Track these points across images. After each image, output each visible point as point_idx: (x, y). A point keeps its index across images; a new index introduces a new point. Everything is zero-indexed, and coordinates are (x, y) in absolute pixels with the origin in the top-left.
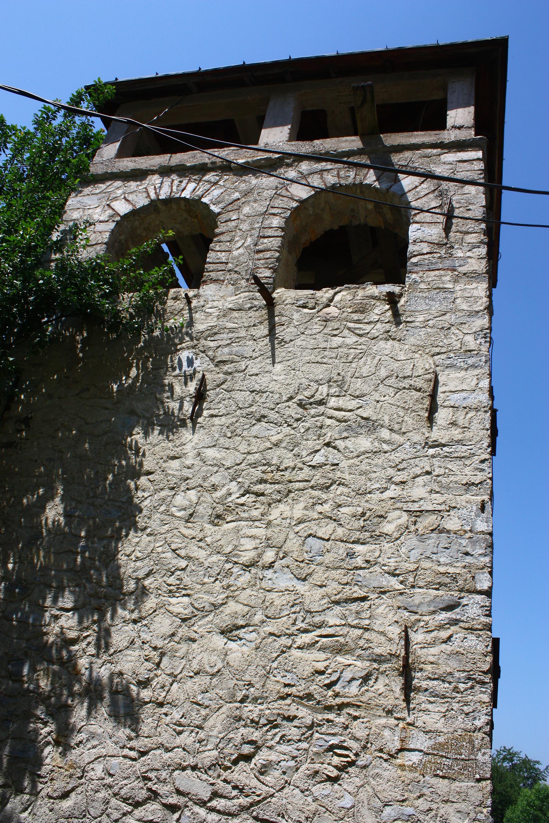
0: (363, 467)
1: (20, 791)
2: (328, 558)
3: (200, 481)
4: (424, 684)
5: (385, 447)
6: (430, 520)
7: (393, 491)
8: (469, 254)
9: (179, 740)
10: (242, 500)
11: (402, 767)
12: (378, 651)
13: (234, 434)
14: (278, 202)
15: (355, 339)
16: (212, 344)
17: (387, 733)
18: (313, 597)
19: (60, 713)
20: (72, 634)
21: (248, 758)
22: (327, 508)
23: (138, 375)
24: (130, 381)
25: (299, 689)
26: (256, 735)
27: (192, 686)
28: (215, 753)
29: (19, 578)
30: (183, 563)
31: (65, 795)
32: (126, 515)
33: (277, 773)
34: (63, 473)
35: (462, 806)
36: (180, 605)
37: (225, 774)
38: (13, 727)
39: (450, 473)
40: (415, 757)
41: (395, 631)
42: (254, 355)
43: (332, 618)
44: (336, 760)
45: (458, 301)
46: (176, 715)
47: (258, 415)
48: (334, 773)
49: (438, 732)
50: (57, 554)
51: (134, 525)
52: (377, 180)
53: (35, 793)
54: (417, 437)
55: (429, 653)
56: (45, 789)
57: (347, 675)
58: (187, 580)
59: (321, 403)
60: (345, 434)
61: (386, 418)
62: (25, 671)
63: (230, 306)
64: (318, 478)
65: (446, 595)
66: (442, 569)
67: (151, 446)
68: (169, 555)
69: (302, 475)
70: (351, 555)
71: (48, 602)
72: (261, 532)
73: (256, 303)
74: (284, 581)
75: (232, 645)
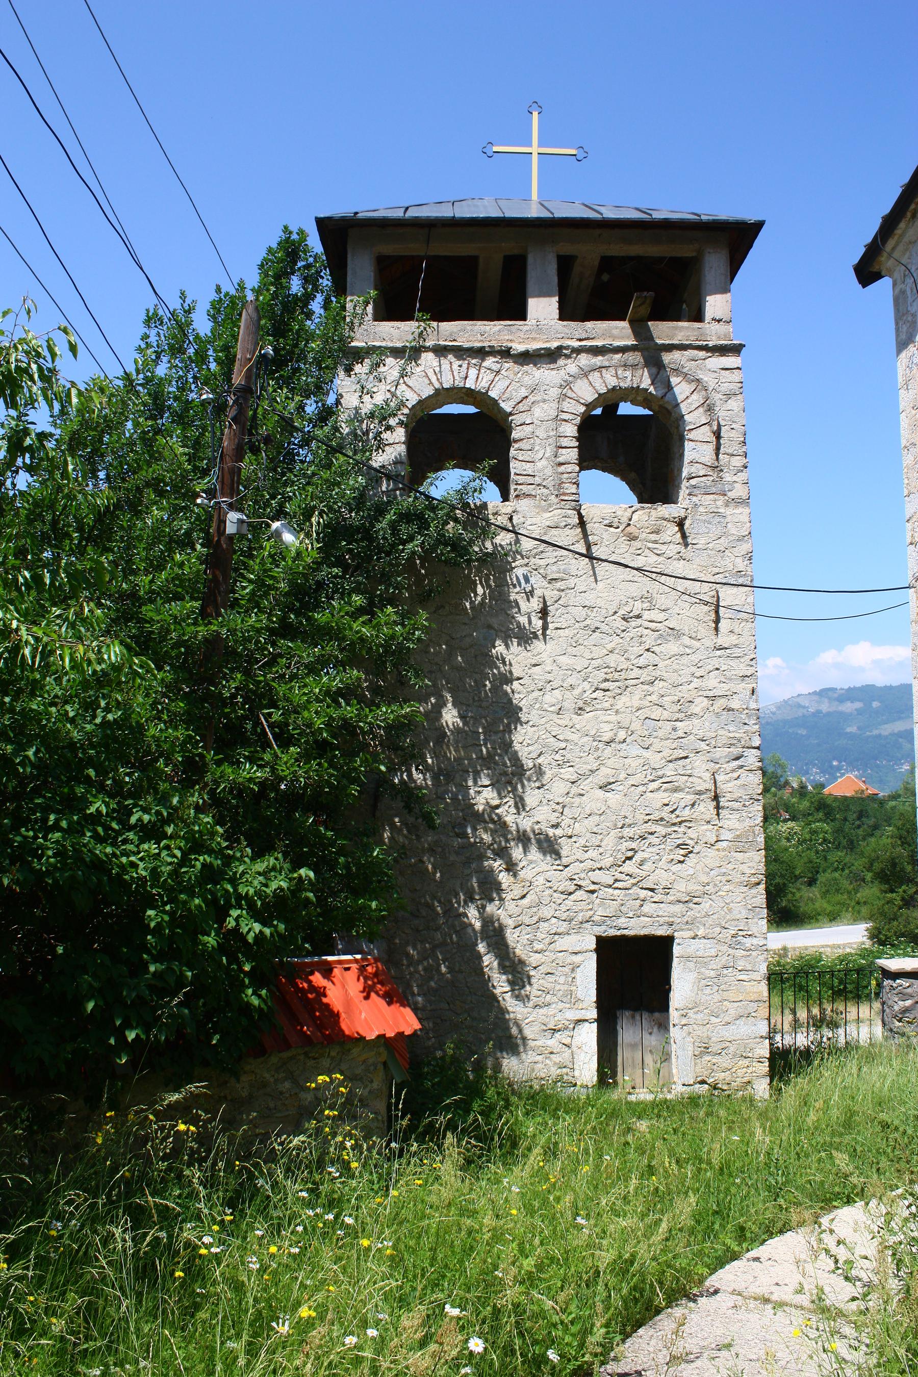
0: (675, 667)
1: (491, 900)
2: (660, 733)
3: (560, 683)
4: (726, 804)
5: (688, 651)
6: (721, 702)
7: (696, 683)
8: (735, 478)
9: (587, 855)
10: (594, 695)
11: (718, 850)
12: (698, 788)
13: (578, 644)
14: (567, 405)
15: (656, 558)
16: (542, 562)
17: (708, 833)
18: (656, 760)
19: (502, 853)
20: (496, 802)
21: (630, 858)
22: (654, 698)
23: (484, 593)
24: (479, 599)
25: (656, 815)
26: (634, 845)
27: (591, 822)
28: (611, 859)
29: (440, 768)
30: (563, 745)
31: (523, 897)
32: (510, 714)
33: (650, 864)
34: (447, 683)
35: (751, 864)
36: (568, 773)
37: (620, 869)
38: (474, 866)
39: (732, 668)
40: (725, 844)
41: (707, 776)
42: (580, 573)
43: (669, 770)
44: (682, 852)
45: (729, 525)
46: (582, 841)
47: (593, 628)
48: (682, 859)
49: (737, 830)
50: (464, 747)
51: (518, 720)
52: (653, 384)
53: (501, 900)
54: (709, 643)
55: (728, 787)
56: (508, 896)
57: (682, 804)
58: (569, 756)
59: (638, 617)
60: (659, 642)
61: (686, 628)
62: (469, 831)
63: (548, 523)
64: (645, 675)
65: (735, 751)
66: (732, 735)
67: (513, 656)
68: (553, 739)
69: (633, 674)
70: (674, 729)
71: (470, 783)
72: (613, 718)
73: (569, 521)
74: (635, 750)
75: (608, 794)
